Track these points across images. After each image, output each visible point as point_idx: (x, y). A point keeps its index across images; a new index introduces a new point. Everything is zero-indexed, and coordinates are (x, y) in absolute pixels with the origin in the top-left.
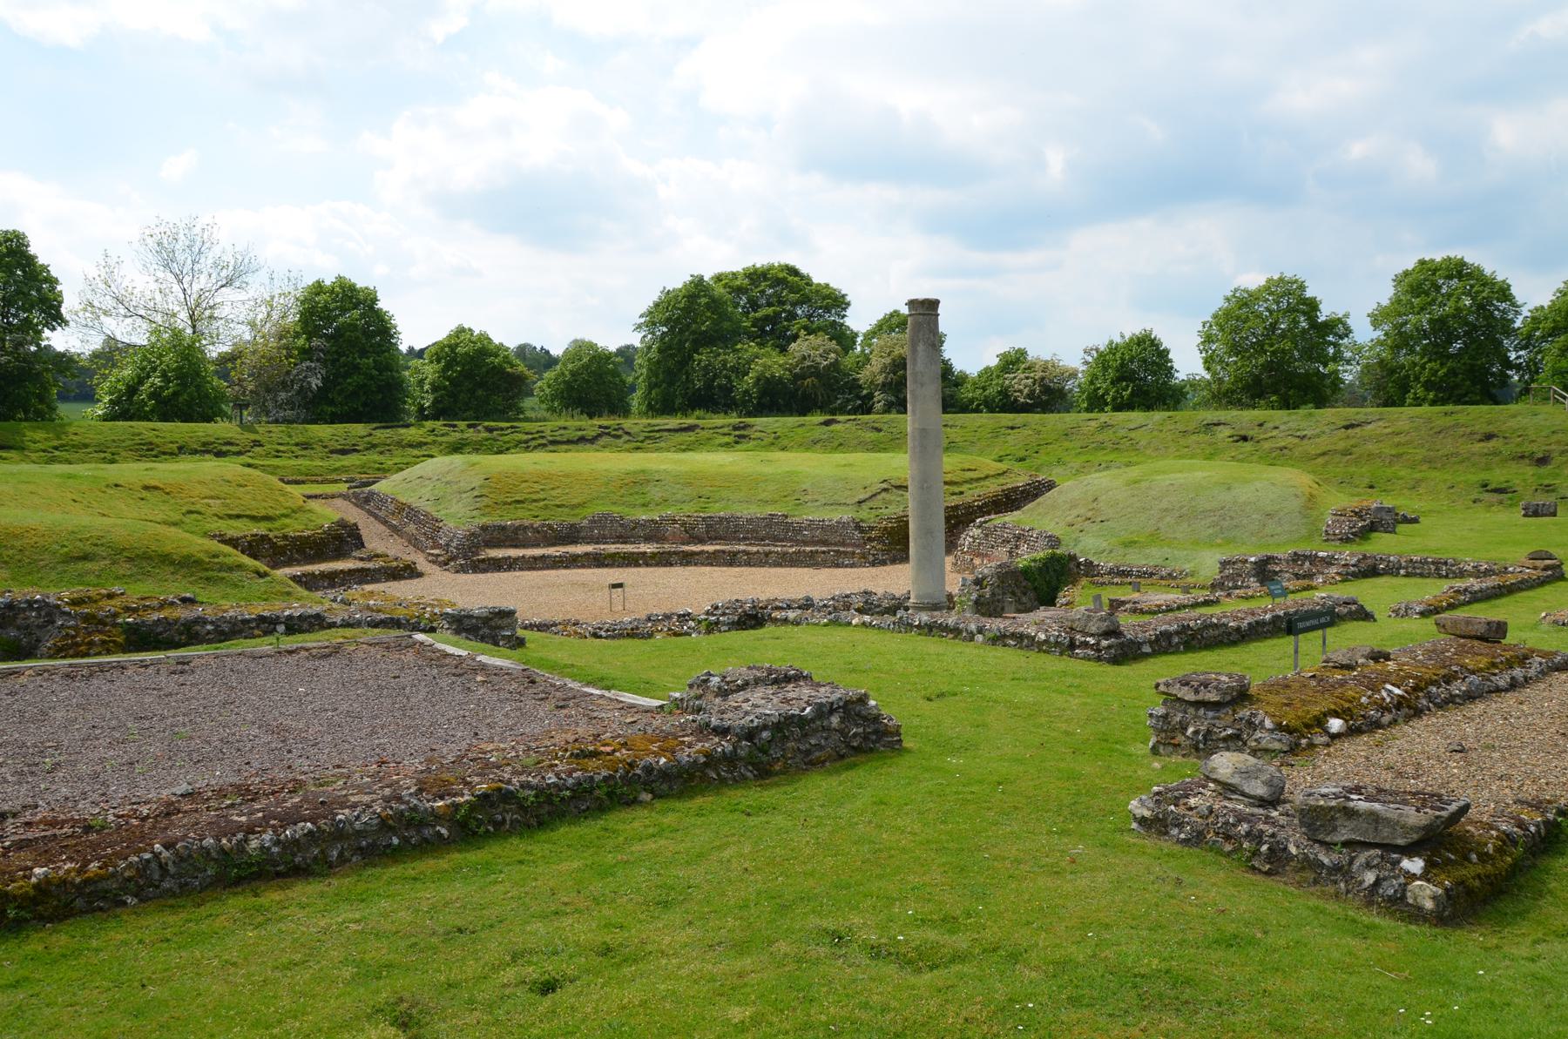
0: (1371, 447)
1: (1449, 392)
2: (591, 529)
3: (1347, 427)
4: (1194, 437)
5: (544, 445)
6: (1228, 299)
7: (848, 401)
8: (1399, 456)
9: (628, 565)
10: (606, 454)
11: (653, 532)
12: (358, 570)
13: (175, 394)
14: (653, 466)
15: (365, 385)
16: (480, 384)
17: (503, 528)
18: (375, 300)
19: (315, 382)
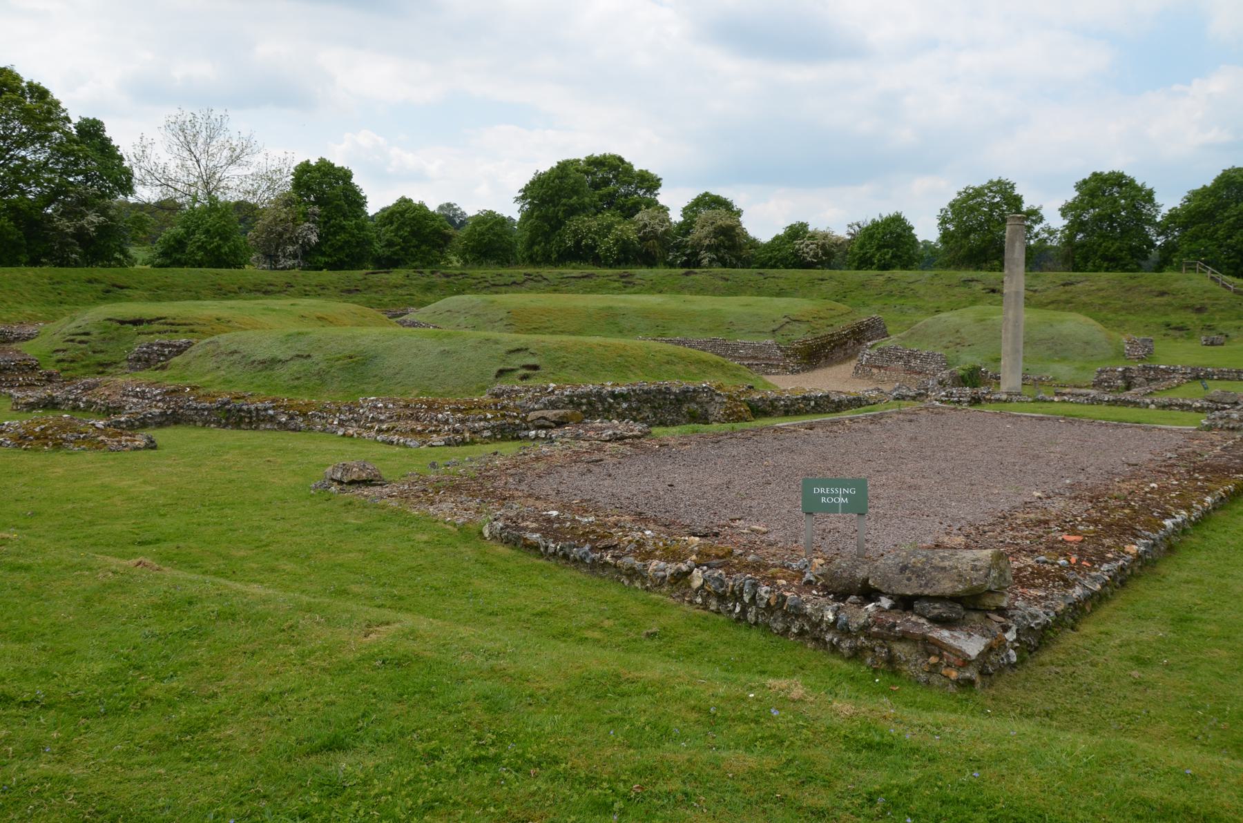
0: (1083, 298)
1: (1113, 262)
3: (1064, 285)
4: (957, 289)
6: (959, 194)
7: (676, 257)
8: (1105, 305)
14: (615, 305)
18: (350, 177)
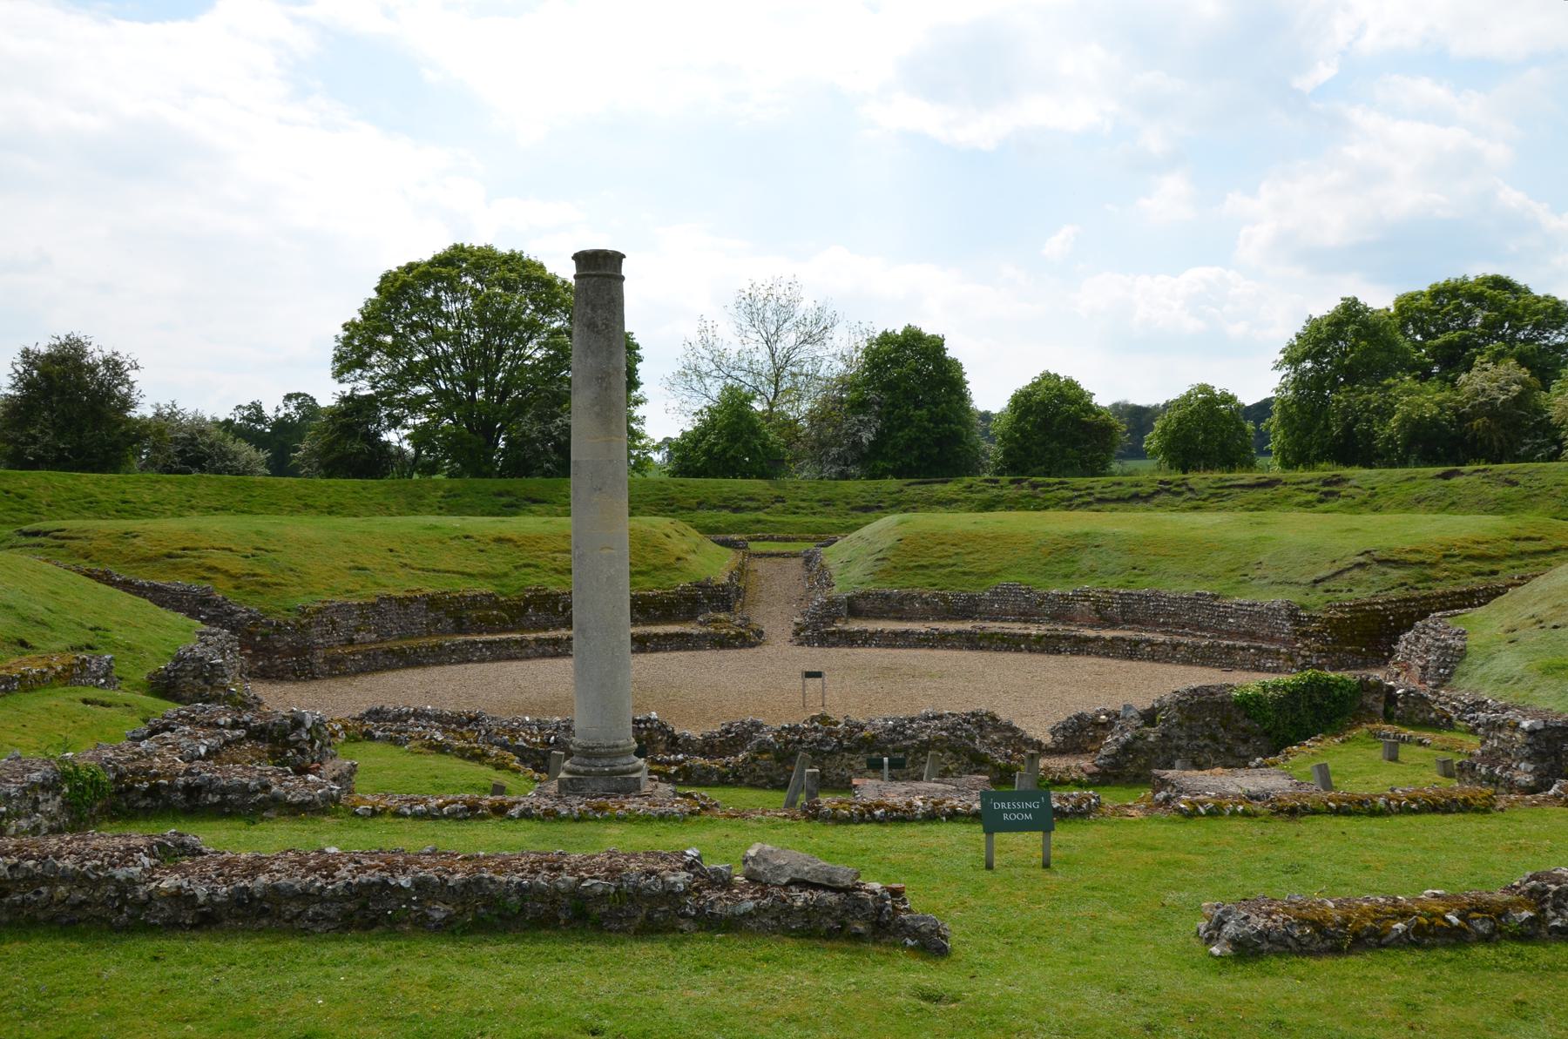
2: (992, 602)
5: (1089, 503)
7: (1541, 446)
9: (1008, 649)
11: (1062, 611)
12: (677, 635)
13: (724, 451)
15: (918, 439)
16: (1061, 434)
17: (887, 597)
19: (867, 436)
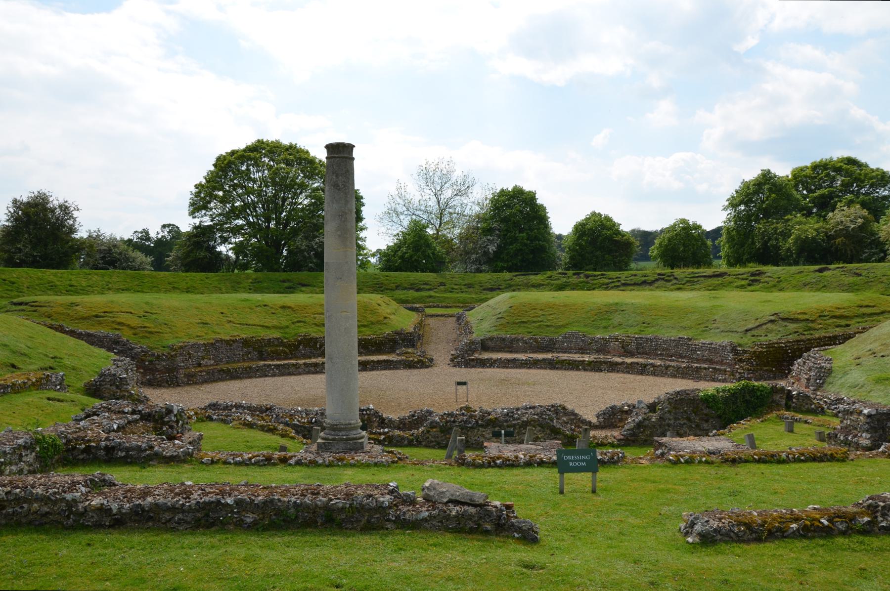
2: (563, 342)
5: (618, 286)
7: (874, 254)
9: (572, 369)
10: (658, 293)
11: (602, 347)
12: (384, 361)
13: (411, 257)
15: (521, 250)
16: (602, 247)
17: (504, 339)
19: (492, 248)
